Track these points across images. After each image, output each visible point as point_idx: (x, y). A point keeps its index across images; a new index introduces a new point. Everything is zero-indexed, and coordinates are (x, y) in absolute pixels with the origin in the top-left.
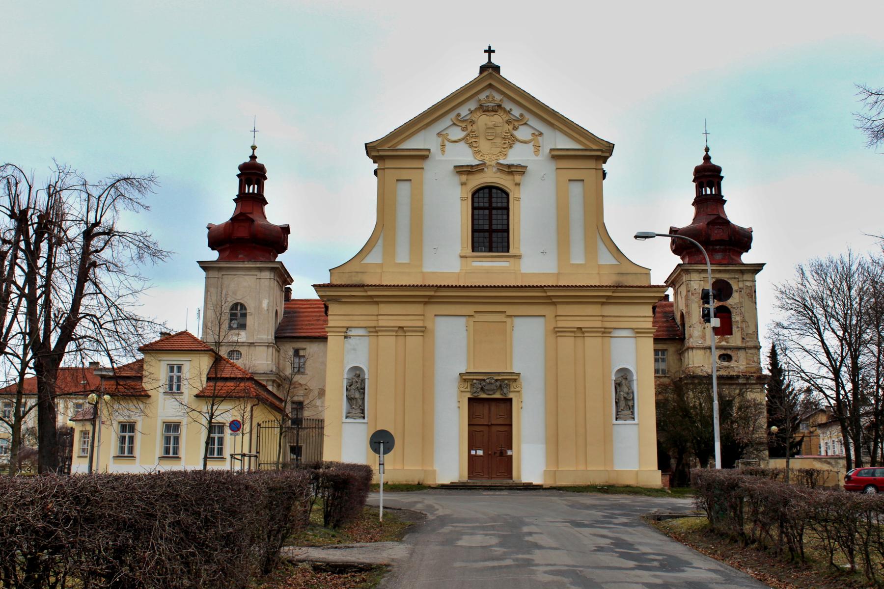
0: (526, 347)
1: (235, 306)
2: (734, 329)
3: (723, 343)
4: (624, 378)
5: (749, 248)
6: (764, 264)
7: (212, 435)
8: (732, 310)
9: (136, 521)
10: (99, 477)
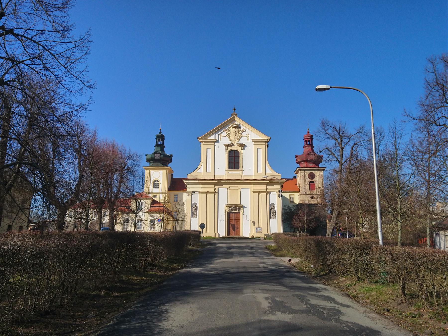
0: (246, 197)
1: (155, 181)
4: (272, 207)
9: (397, 257)
10: (138, 233)
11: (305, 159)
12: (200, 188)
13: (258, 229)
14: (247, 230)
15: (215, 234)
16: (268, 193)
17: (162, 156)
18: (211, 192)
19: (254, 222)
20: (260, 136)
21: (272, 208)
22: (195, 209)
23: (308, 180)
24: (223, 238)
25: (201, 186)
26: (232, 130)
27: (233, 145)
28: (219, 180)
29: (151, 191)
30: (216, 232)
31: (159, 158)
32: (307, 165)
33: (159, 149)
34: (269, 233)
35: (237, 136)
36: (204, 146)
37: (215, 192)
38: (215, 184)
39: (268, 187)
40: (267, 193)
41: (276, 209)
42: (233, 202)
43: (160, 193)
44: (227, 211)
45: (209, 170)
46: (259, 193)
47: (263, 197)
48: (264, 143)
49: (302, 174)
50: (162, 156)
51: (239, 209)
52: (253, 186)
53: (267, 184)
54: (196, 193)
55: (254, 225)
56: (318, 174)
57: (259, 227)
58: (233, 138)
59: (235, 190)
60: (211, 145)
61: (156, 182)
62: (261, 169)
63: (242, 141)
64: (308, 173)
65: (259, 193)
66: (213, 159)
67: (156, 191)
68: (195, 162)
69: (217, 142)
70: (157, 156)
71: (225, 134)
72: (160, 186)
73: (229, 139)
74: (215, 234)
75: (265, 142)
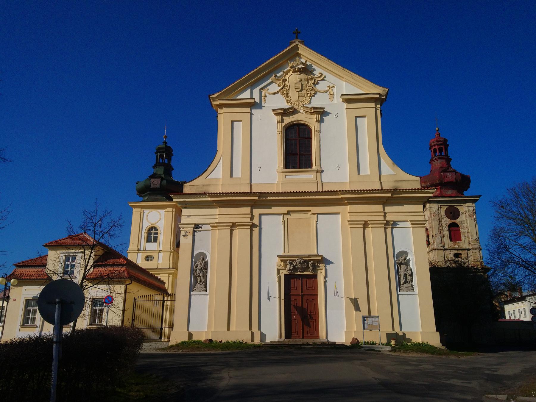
0: (331, 235)
1: (151, 229)
2: (463, 238)
3: (456, 246)
4: (402, 262)
5: (469, 187)
6: (332, 263)
7: (29, 308)
8: (144, 330)
11: (437, 181)
12: (214, 215)
13: (369, 321)
14: (337, 326)
15: (253, 334)
16: (390, 225)
17: (164, 182)
18: (243, 225)
19: (355, 302)
20: (360, 88)
21: (401, 264)
22: (201, 270)
23: (446, 221)
24: (273, 346)
25: (217, 211)
26: (292, 78)
27: (293, 111)
28: (260, 194)
29: (142, 249)
30: (255, 329)
31: (158, 186)
32: (441, 193)
33: (161, 171)
34: (397, 330)
35: (304, 92)
36: (224, 118)
37: (253, 226)
38: (253, 205)
39: (388, 209)
40: (387, 224)
41: (412, 265)
42: (302, 248)
43: (160, 251)
44: (283, 273)
45: (238, 172)
46: (365, 224)
47: (375, 234)
48: (373, 105)
49: (434, 210)
50: (164, 182)
51: (315, 268)
52: (348, 208)
53: (386, 202)
54: (204, 227)
55: (357, 309)
56: (466, 210)
57: (370, 316)
58: (294, 95)
59: (305, 218)
60: (242, 114)
61: (153, 232)
62: (367, 168)
63: (317, 102)
64: (446, 208)
65: (365, 224)
66: (247, 143)
67: (152, 246)
68: (205, 152)
69: (254, 105)
70: (156, 183)
71: (274, 88)
72: (161, 238)
73: (285, 100)
74: (253, 334)
75: (375, 100)
